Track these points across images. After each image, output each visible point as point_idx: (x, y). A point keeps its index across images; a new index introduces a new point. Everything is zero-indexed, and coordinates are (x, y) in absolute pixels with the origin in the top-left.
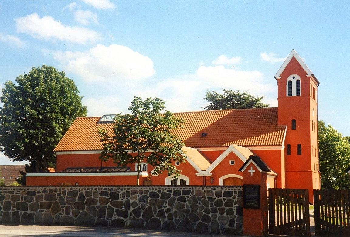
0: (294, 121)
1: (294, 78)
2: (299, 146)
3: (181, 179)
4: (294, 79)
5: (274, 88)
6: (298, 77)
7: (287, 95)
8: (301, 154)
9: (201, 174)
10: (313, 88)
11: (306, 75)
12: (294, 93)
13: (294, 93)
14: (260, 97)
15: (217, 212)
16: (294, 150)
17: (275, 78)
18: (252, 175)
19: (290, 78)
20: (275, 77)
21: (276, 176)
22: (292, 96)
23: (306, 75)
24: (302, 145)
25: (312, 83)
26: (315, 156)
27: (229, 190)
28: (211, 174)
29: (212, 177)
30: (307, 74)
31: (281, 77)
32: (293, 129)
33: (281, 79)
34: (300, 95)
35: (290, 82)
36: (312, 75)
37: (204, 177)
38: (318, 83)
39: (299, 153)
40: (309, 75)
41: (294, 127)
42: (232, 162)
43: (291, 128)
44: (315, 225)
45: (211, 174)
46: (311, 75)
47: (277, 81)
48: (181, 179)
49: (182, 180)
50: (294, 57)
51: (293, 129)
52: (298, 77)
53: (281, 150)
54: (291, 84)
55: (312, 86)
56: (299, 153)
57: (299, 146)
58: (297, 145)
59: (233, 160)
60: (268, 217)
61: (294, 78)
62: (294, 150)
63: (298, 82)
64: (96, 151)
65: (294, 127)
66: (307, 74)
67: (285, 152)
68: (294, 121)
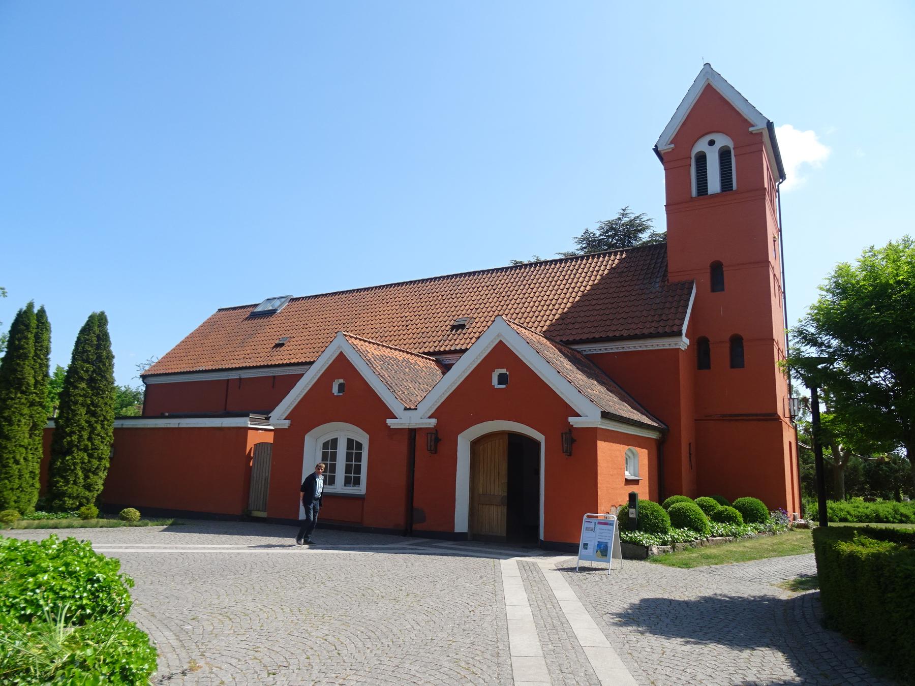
0: (717, 269)
1: (712, 143)
3: (348, 439)
6: (723, 141)
9: (403, 420)
11: (751, 129)
12: (714, 184)
13: (714, 184)
17: (656, 150)
19: (701, 146)
20: (656, 146)
22: (709, 194)
23: (751, 129)
27: (351, 490)
28: (434, 421)
30: (753, 126)
31: (673, 146)
32: (733, 366)
34: (735, 187)
35: (701, 159)
42: (502, 379)
43: (709, 290)
44: (818, 572)
45: (434, 421)
46: (765, 126)
48: (348, 439)
49: (353, 440)
51: (733, 366)
52: (723, 141)
54: (706, 160)
57: (736, 342)
59: (504, 371)
62: (720, 354)
63: (724, 155)
64: (272, 369)
66: (753, 126)
67: (371, 550)
68: (717, 269)
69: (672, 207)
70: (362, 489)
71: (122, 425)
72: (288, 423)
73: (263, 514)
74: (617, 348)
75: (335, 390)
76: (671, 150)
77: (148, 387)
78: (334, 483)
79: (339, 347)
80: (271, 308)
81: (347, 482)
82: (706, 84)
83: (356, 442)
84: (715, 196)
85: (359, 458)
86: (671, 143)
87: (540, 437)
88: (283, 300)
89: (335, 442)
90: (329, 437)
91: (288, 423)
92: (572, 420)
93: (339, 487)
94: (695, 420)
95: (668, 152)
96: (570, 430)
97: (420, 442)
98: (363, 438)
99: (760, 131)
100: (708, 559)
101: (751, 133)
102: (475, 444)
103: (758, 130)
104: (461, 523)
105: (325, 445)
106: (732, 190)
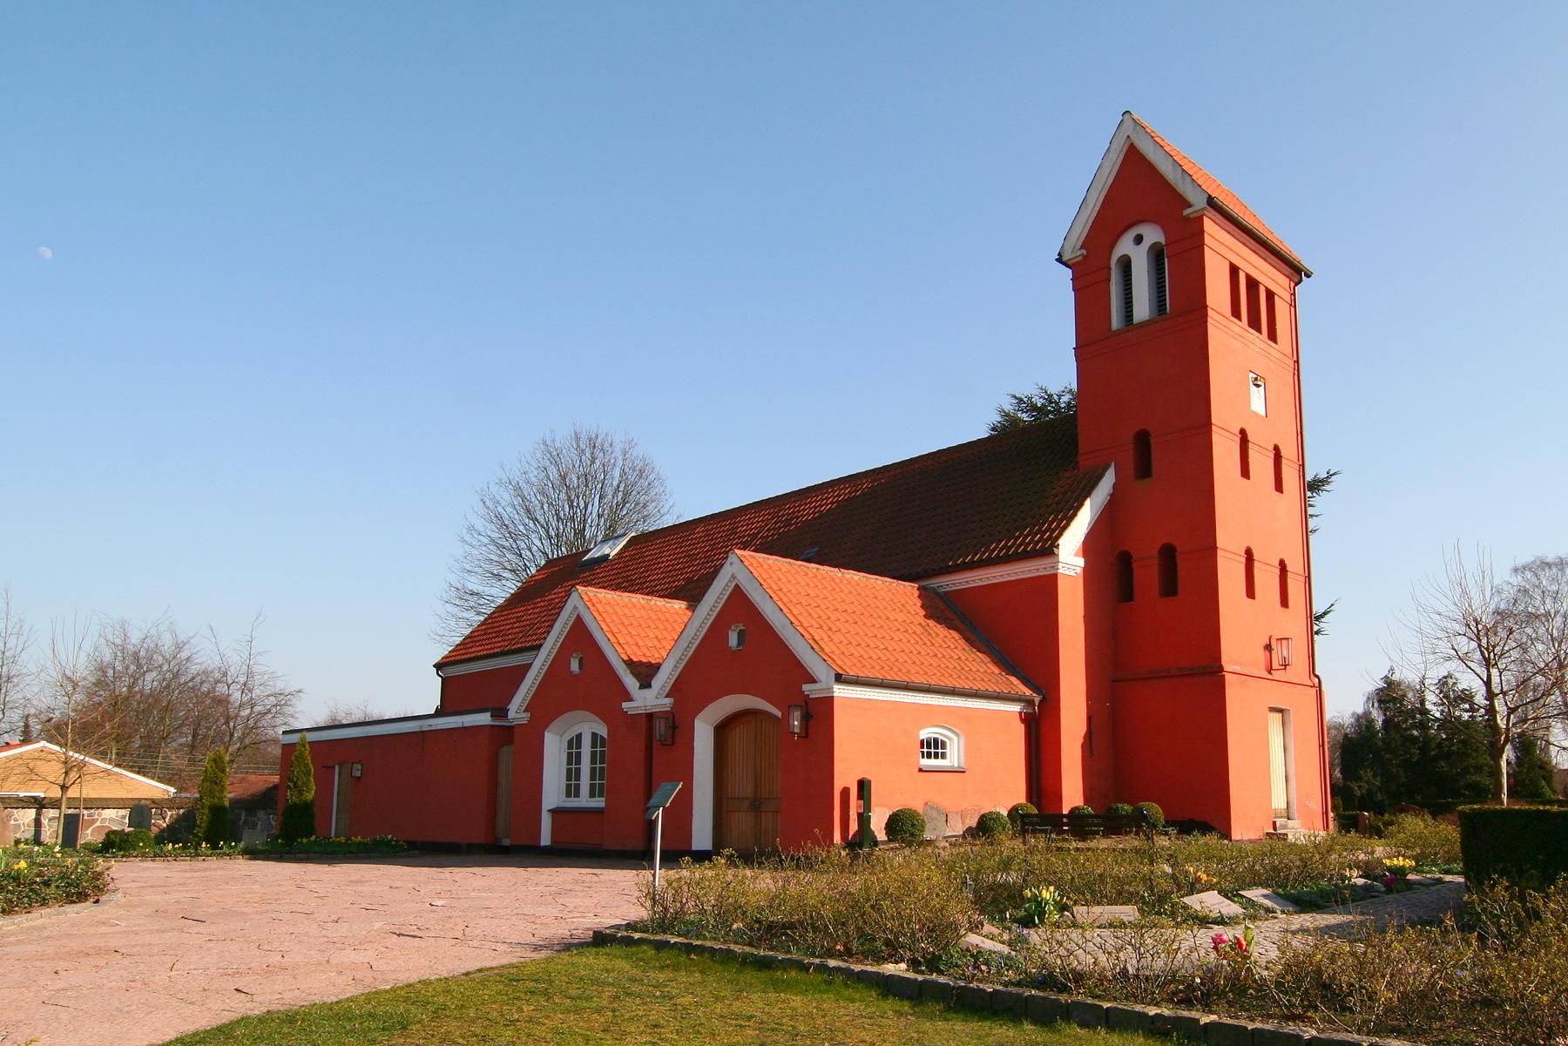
0: (1143, 441)
1: (1139, 240)
2: (1168, 555)
7: (1116, 322)
10: (1253, 284)
12: (1142, 309)
14: (1323, 475)
15: (555, 812)
16: (1147, 575)
17: (1060, 260)
19: (1125, 246)
20: (1059, 254)
21: (1030, 702)
23: (1186, 212)
24: (1178, 549)
26: (1284, 602)
33: (1085, 257)
35: (1126, 264)
36: (1211, 202)
37: (650, 717)
38: (1296, 272)
39: (1170, 586)
40: (1199, 202)
41: (1144, 468)
45: (669, 701)
47: (1068, 273)
52: (1153, 234)
53: (1055, 576)
56: (1170, 586)
57: (1168, 555)
60: (671, 799)
62: (1147, 575)
63: (1157, 254)
65: (1144, 468)
66: (1189, 205)
68: (1143, 441)
71: (421, 727)
72: (669, 701)
74: (1002, 575)
76: (1080, 258)
77: (444, 681)
78: (579, 796)
83: (601, 736)
84: (1143, 324)
86: (1082, 248)
89: (579, 737)
90: (572, 733)
92: (806, 688)
93: (584, 800)
94: (1114, 681)
95: (1077, 262)
96: (806, 702)
97: (660, 728)
99: (1199, 214)
100: (409, 856)
102: (722, 730)
103: (1196, 212)
104: (546, 839)
105: (570, 743)
106: (1166, 313)
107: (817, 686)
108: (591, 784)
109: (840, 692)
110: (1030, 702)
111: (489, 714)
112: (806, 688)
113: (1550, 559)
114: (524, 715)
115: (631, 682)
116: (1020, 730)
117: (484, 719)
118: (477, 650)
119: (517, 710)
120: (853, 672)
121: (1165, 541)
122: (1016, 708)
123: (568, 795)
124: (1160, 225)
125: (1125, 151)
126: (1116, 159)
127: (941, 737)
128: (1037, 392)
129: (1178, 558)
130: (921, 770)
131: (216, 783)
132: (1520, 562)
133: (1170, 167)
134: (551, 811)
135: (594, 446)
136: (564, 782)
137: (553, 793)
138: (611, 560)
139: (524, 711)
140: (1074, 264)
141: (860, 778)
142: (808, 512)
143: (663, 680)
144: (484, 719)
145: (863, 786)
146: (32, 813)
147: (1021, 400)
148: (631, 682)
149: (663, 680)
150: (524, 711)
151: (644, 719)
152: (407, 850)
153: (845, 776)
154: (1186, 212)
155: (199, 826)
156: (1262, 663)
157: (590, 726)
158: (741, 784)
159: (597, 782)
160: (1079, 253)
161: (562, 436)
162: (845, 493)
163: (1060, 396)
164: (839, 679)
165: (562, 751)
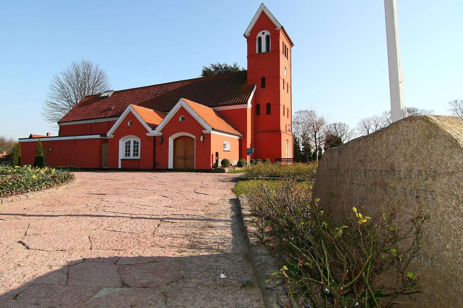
0: (263, 79)
1: (263, 33)
2: (269, 105)
4: (263, 35)
5: (243, 45)
6: (267, 33)
7: (257, 52)
8: (270, 114)
10: (285, 46)
12: (264, 50)
13: (264, 50)
15: (122, 160)
16: (263, 110)
17: (244, 35)
18: (248, 156)
19: (260, 34)
23: (276, 29)
25: (282, 38)
27: (136, 158)
28: (161, 133)
29: (161, 137)
30: (149, 133)
33: (250, 36)
35: (260, 39)
36: (282, 27)
37: (155, 137)
38: (292, 44)
39: (268, 112)
40: (279, 27)
42: (183, 119)
43: (260, 87)
45: (161, 133)
50: (263, 11)
52: (267, 33)
53: (247, 108)
55: (283, 43)
56: (268, 112)
57: (269, 105)
58: (266, 105)
59: (183, 116)
61: (263, 33)
62: (263, 110)
63: (268, 38)
68: (263, 79)
69: (249, 57)
70: (139, 157)
71: (74, 138)
72: (113, 136)
73: (107, 168)
75: (129, 124)
77: (60, 127)
79: (130, 109)
80: (107, 95)
81: (134, 155)
82: (262, 11)
84: (264, 53)
85: (138, 147)
87: (194, 137)
88: (111, 92)
89: (129, 142)
90: (128, 140)
91: (113, 136)
92: (203, 131)
93: (132, 157)
94: (255, 133)
98: (139, 140)
99: (279, 30)
101: (276, 30)
102: (175, 141)
104: (120, 167)
105: (126, 143)
107: (207, 131)
108: (134, 153)
109: (213, 132)
110: (240, 136)
111: (99, 135)
112: (203, 131)
113: (303, 110)
114: (113, 136)
115: (149, 129)
116: (238, 143)
117: (98, 136)
118: (71, 119)
119: (110, 134)
120: (215, 128)
121: (268, 102)
122: (238, 137)
123: (126, 155)
124: (269, 31)
125: (261, 12)
126: (259, 14)
127: (225, 144)
128: (217, 64)
129: (271, 106)
130: (224, 151)
131: (18, 152)
132: (297, 111)
133: (273, 18)
134: (121, 160)
135: (88, 66)
136: (125, 153)
137: (122, 155)
138: (110, 97)
139: (112, 135)
140: (248, 37)
141: (218, 152)
142: (171, 89)
143: (158, 129)
144: (98, 136)
145: (217, 154)
146: (315, 141)
147: (213, 65)
148: (149, 129)
149: (158, 129)
150: (112, 135)
151: (153, 138)
152: (80, 169)
153: (213, 152)
154: (276, 29)
155: (14, 163)
156: (285, 130)
157: (132, 139)
158: (181, 153)
159: (128, 153)
160: (249, 34)
161: (79, 62)
162: (181, 85)
163: (222, 65)
164: (213, 129)
165: (124, 144)
